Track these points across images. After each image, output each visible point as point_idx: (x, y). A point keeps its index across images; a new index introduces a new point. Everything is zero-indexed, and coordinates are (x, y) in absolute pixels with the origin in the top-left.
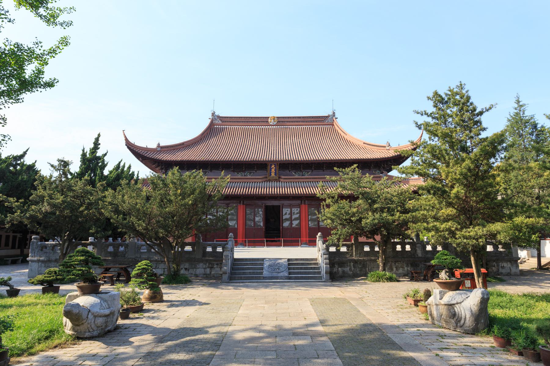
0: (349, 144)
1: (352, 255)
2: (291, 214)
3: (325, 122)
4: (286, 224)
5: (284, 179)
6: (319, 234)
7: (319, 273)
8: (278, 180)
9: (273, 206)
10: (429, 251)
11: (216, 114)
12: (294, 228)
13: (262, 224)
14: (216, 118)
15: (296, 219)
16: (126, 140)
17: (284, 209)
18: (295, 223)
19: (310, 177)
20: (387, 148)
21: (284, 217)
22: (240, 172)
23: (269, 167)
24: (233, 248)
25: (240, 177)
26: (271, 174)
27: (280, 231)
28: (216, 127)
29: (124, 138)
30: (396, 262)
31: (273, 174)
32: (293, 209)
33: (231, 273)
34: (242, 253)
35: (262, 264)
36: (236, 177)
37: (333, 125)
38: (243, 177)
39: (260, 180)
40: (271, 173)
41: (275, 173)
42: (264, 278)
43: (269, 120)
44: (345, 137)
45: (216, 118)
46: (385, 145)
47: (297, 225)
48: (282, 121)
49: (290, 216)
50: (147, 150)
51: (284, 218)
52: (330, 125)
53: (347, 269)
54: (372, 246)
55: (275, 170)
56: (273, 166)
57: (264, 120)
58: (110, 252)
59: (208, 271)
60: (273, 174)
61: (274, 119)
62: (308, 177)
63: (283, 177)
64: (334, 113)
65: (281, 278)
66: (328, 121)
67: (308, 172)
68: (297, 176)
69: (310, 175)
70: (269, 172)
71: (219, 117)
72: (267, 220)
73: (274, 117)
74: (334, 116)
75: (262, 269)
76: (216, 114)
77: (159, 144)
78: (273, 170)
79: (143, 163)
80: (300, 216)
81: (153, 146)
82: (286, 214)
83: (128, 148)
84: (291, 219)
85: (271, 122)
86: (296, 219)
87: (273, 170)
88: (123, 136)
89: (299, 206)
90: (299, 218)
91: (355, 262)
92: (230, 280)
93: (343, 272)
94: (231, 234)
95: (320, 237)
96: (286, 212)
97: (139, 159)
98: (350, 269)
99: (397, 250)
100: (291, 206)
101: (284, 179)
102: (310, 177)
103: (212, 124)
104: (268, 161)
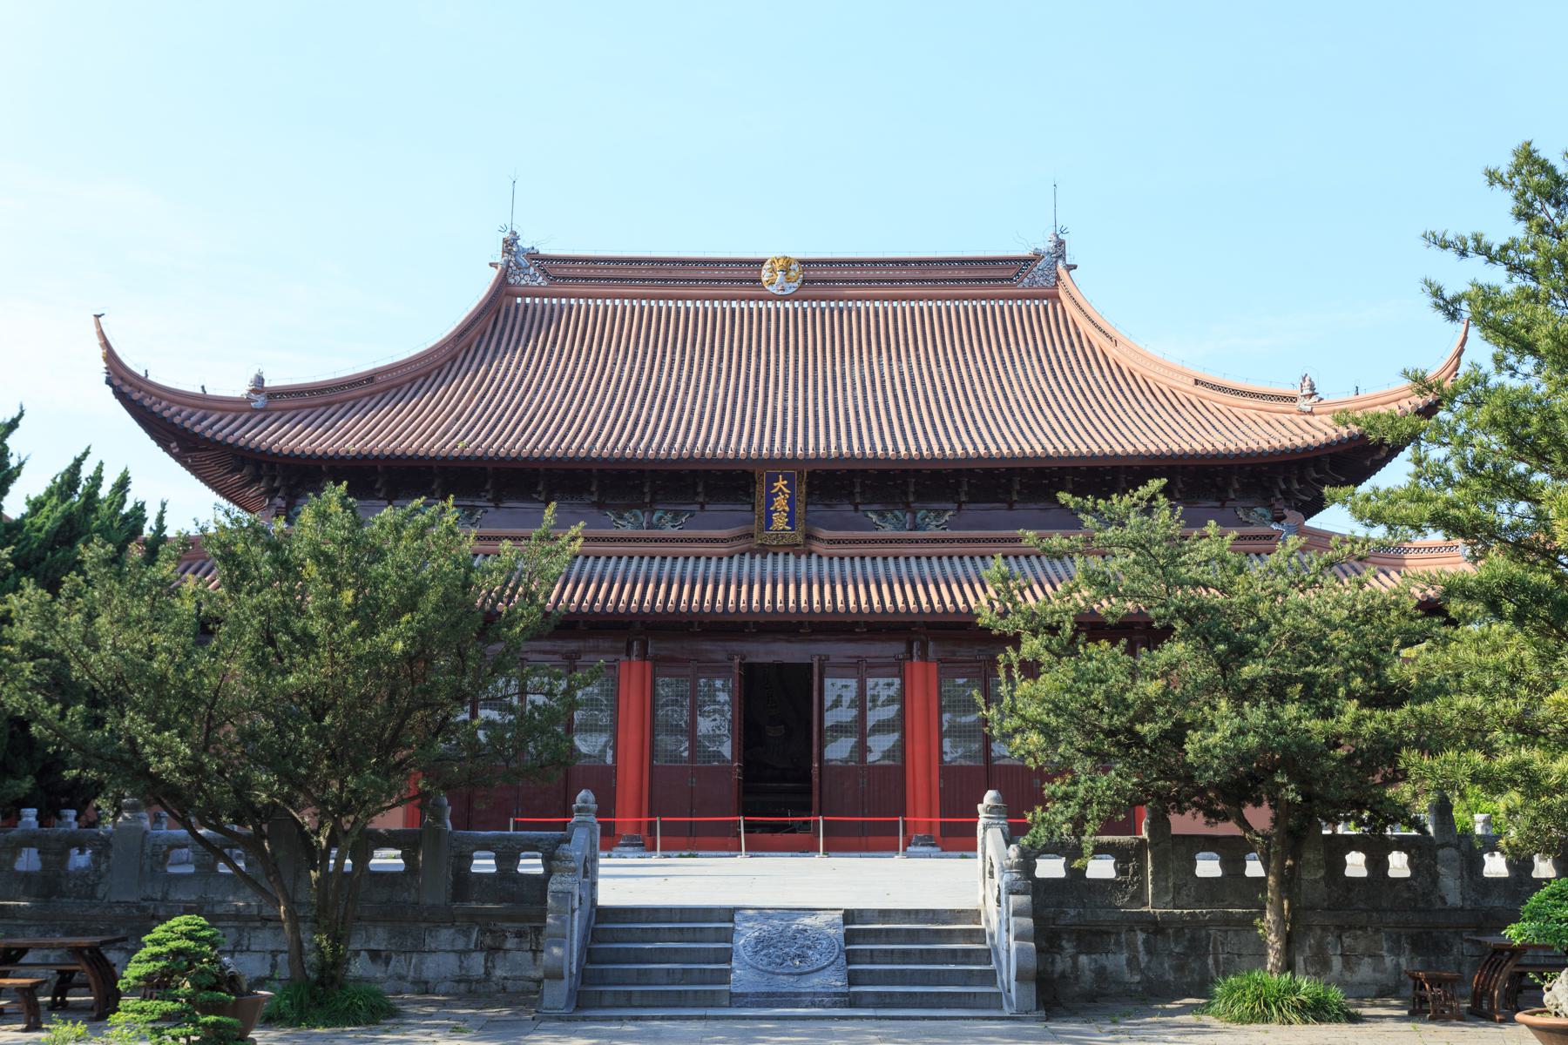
0: (1128, 384)
1: (1139, 897)
2: (861, 702)
3: (1018, 283)
4: (838, 750)
5: (831, 541)
6: (990, 796)
7: (990, 977)
8: (802, 548)
10: (1497, 882)
12: (874, 768)
13: (726, 750)
14: (523, 261)
15: (883, 727)
16: (111, 357)
17: (828, 682)
18: (880, 745)
19: (949, 533)
20: (1305, 404)
21: (830, 719)
22: (629, 508)
23: (761, 490)
24: (594, 860)
25: (628, 530)
26: (770, 522)
28: (522, 305)
29: (99, 352)
30: (1341, 929)
31: (780, 521)
33: (584, 977)
34: (633, 881)
35: (728, 935)
37: (1055, 298)
38: (645, 533)
39: (722, 549)
40: (769, 514)
41: (791, 515)
42: (736, 999)
43: (765, 275)
44: (1112, 353)
45: (523, 261)
46: (1296, 391)
47: (887, 754)
48: (823, 279)
49: (858, 715)
51: (827, 724)
52: (1041, 297)
53: (1116, 961)
54: (1232, 852)
55: (790, 502)
56: (781, 484)
57: (739, 275)
58: (27, 877)
59: (477, 963)
60: (780, 521)
61: (786, 270)
63: (825, 534)
64: (1060, 244)
65: (814, 999)
66: (1033, 281)
67: (940, 513)
68: (888, 532)
69: (950, 525)
70: (760, 509)
71: (534, 257)
72: (749, 731)
73: (788, 261)
74: (1062, 256)
75: (727, 956)
76: (525, 243)
77: (260, 380)
78: (781, 503)
79: (184, 464)
80: (902, 713)
81: (234, 386)
83: (119, 394)
86: (883, 727)
87: (781, 503)
88: (97, 341)
89: (898, 667)
90: (899, 724)
91: (1155, 927)
92: (578, 1007)
93: (1101, 972)
94: (584, 796)
95: (991, 810)
96: (838, 692)
97: (167, 449)
98: (1132, 962)
99: (1349, 873)
100: (861, 669)
101: (831, 541)
102: (949, 533)
103: (502, 291)
104: (760, 461)
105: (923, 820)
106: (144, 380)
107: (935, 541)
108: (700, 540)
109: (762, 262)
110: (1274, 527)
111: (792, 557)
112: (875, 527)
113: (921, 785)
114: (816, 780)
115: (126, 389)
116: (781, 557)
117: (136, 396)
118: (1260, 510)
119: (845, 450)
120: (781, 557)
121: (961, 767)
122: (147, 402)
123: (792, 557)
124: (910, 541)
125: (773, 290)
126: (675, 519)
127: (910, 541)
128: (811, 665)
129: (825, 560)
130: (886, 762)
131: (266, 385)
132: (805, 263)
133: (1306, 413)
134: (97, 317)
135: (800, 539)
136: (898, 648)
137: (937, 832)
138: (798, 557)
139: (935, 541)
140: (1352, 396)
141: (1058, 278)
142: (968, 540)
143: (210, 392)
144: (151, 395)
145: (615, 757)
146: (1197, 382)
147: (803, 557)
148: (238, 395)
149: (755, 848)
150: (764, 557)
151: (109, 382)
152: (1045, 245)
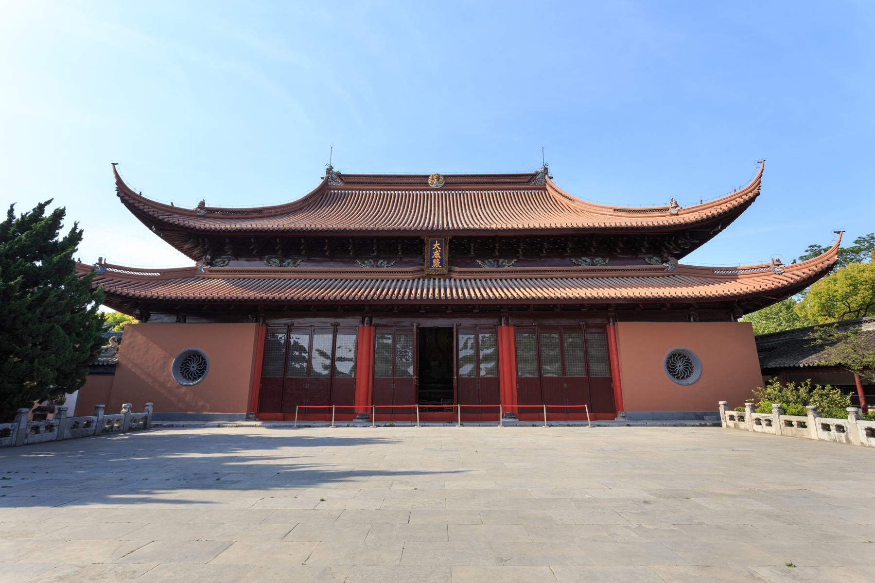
2: (477, 347)
3: (531, 184)
4: (465, 370)
5: (460, 272)
9: (437, 330)
11: (335, 170)
12: (483, 378)
13: (411, 370)
14: (334, 176)
15: (487, 359)
16: (120, 183)
17: (460, 336)
21: (461, 354)
22: (367, 259)
23: (427, 248)
25: (367, 268)
26: (432, 263)
27: (452, 388)
28: (333, 189)
31: (436, 263)
32: (565, 336)
36: (363, 269)
37: (545, 189)
38: (374, 269)
39: (410, 276)
40: (431, 260)
41: (441, 261)
43: (430, 181)
45: (334, 176)
46: (669, 205)
47: (489, 371)
49: (474, 352)
50: (172, 210)
51: (460, 357)
55: (441, 254)
56: (436, 245)
57: (419, 182)
60: (436, 263)
62: (510, 269)
63: (457, 269)
64: (546, 169)
66: (536, 183)
68: (487, 268)
69: (514, 265)
72: (422, 363)
74: (547, 173)
76: (335, 170)
77: (202, 204)
78: (437, 254)
79: (159, 235)
80: (497, 351)
81: (192, 206)
82: (465, 347)
83: (123, 201)
84: (476, 360)
85: (433, 183)
86: (487, 359)
87: (437, 254)
88: (114, 175)
89: (494, 330)
90: (496, 357)
97: (151, 229)
101: (460, 272)
105: (509, 406)
106: (140, 196)
107: (509, 272)
108: (400, 272)
109: (428, 176)
110: (665, 264)
111: (442, 280)
112: (480, 266)
113: (508, 388)
114: (455, 385)
115: (126, 198)
116: (437, 280)
117: (131, 201)
118: (655, 258)
119: (450, 226)
120: (437, 280)
121: (527, 378)
122: (136, 205)
123: (442, 280)
124: (497, 272)
125: (433, 186)
126: (388, 263)
127: (497, 272)
128: (452, 328)
129: (458, 281)
130: (490, 376)
131: (206, 206)
132: (445, 176)
133: (674, 215)
134: (114, 164)
135: (446, 272)
136: (491, 321)
137: (516, 411)
138: (445, 280)
139: (509, 272)
140: (699, 204)
141: (546, 181)
142: (524, 271)
143: (175, 205)
144: (145, 204)
145: (355, 375)
146: (615, 210)
147: (447, 280)
148: (191, 209)
149: (426, 420)
150: (429, 280)
151: (118, 195)
152: (540, 169)
